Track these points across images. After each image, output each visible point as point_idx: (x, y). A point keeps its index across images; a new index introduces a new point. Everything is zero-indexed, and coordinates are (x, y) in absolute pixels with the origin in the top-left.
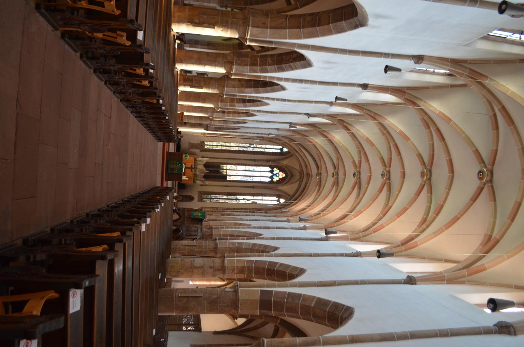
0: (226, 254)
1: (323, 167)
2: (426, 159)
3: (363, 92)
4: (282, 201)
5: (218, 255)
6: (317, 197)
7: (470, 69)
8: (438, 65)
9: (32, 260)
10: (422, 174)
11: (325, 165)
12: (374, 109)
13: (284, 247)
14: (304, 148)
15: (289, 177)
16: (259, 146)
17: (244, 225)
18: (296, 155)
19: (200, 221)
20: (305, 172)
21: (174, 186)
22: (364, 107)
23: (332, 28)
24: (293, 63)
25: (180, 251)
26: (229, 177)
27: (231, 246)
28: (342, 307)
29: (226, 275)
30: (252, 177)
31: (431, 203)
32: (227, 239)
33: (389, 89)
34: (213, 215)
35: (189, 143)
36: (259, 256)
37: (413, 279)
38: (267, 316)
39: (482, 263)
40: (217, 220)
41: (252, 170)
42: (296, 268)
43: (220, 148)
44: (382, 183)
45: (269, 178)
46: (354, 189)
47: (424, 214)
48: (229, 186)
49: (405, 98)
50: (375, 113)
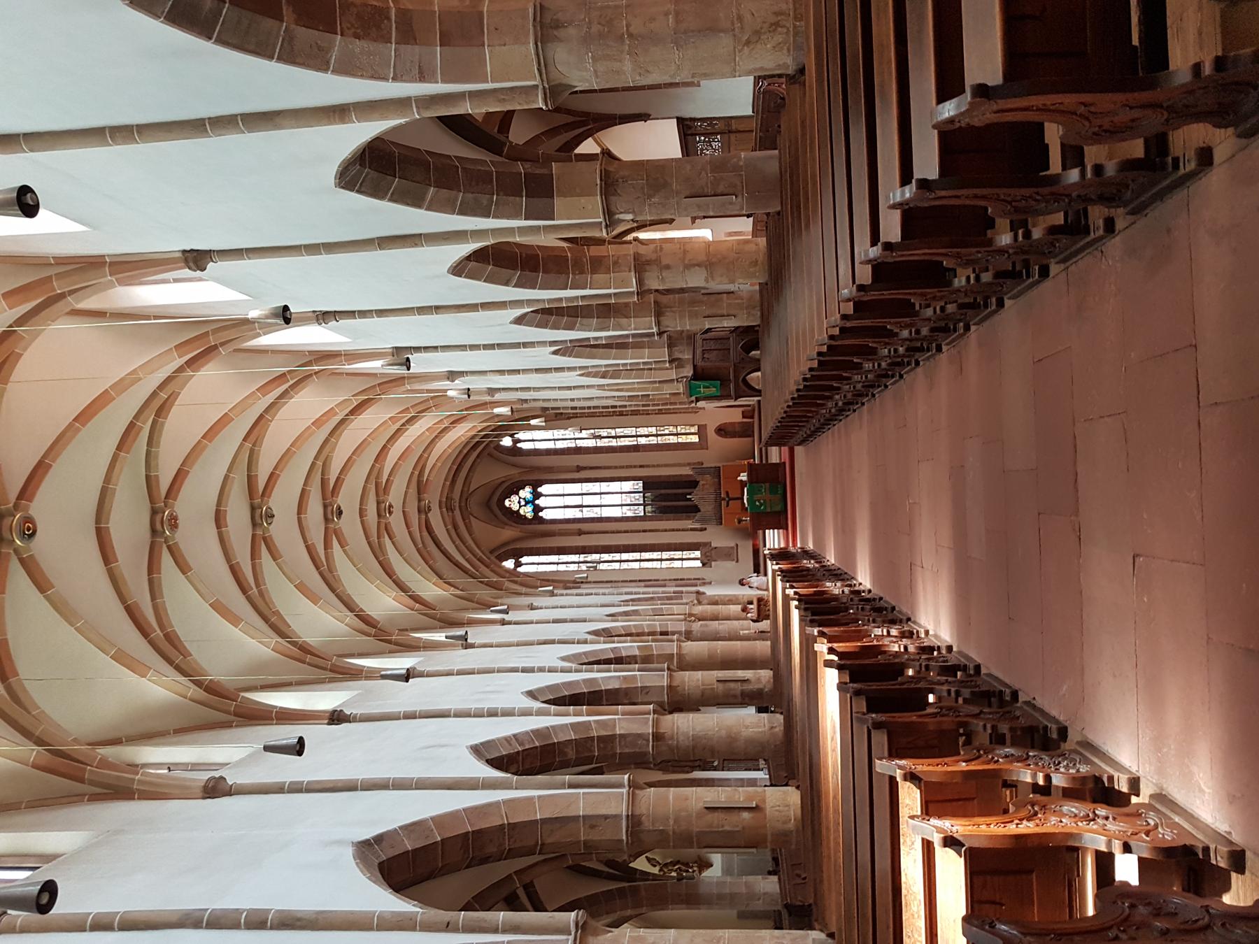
0: (636, 299)
1: (415, 528)
2: (166, 560)
3: (339, 706)
4: (507, 442)
5: (652, 297)
6: (426, 455)
7: (82, 781)
8: (165, 781)
9: (1020, 232)
10: (174, 523)
11: (410, 533)
12: (306, 672)
13: (500, 325)
14: (465, 571)
15: (495, 498)
16: (573, 567)
17: (595, 375)
18: (482, 552)
19: (699, 375)
20: (457, 512)
21: (763, 449)
22: (333, 675)
23: (435, 831)
24: (516, 750)
25: (740, 301)
26: (637, 487)
27: (624, 321)
28: (363, 189)
29: (632, 253)
30: (584, 492)
31: (148, 454)
32: (634, 336)
33: (277, 720)
34: (670, 394)
35: (737, 561)
36: (560, 300)
37: (191, 264)
38: (534, 160)
39: (14, 310)
40: (660, 382)
41: (584, 509)
42: (472, 276)
43: (666, 555)
44: (269, 497)
45: (544, 493)
46: (338, 478)
47: (163, 424)
48: (635, 467)
49: (233, 701)
50: (304, 662)
